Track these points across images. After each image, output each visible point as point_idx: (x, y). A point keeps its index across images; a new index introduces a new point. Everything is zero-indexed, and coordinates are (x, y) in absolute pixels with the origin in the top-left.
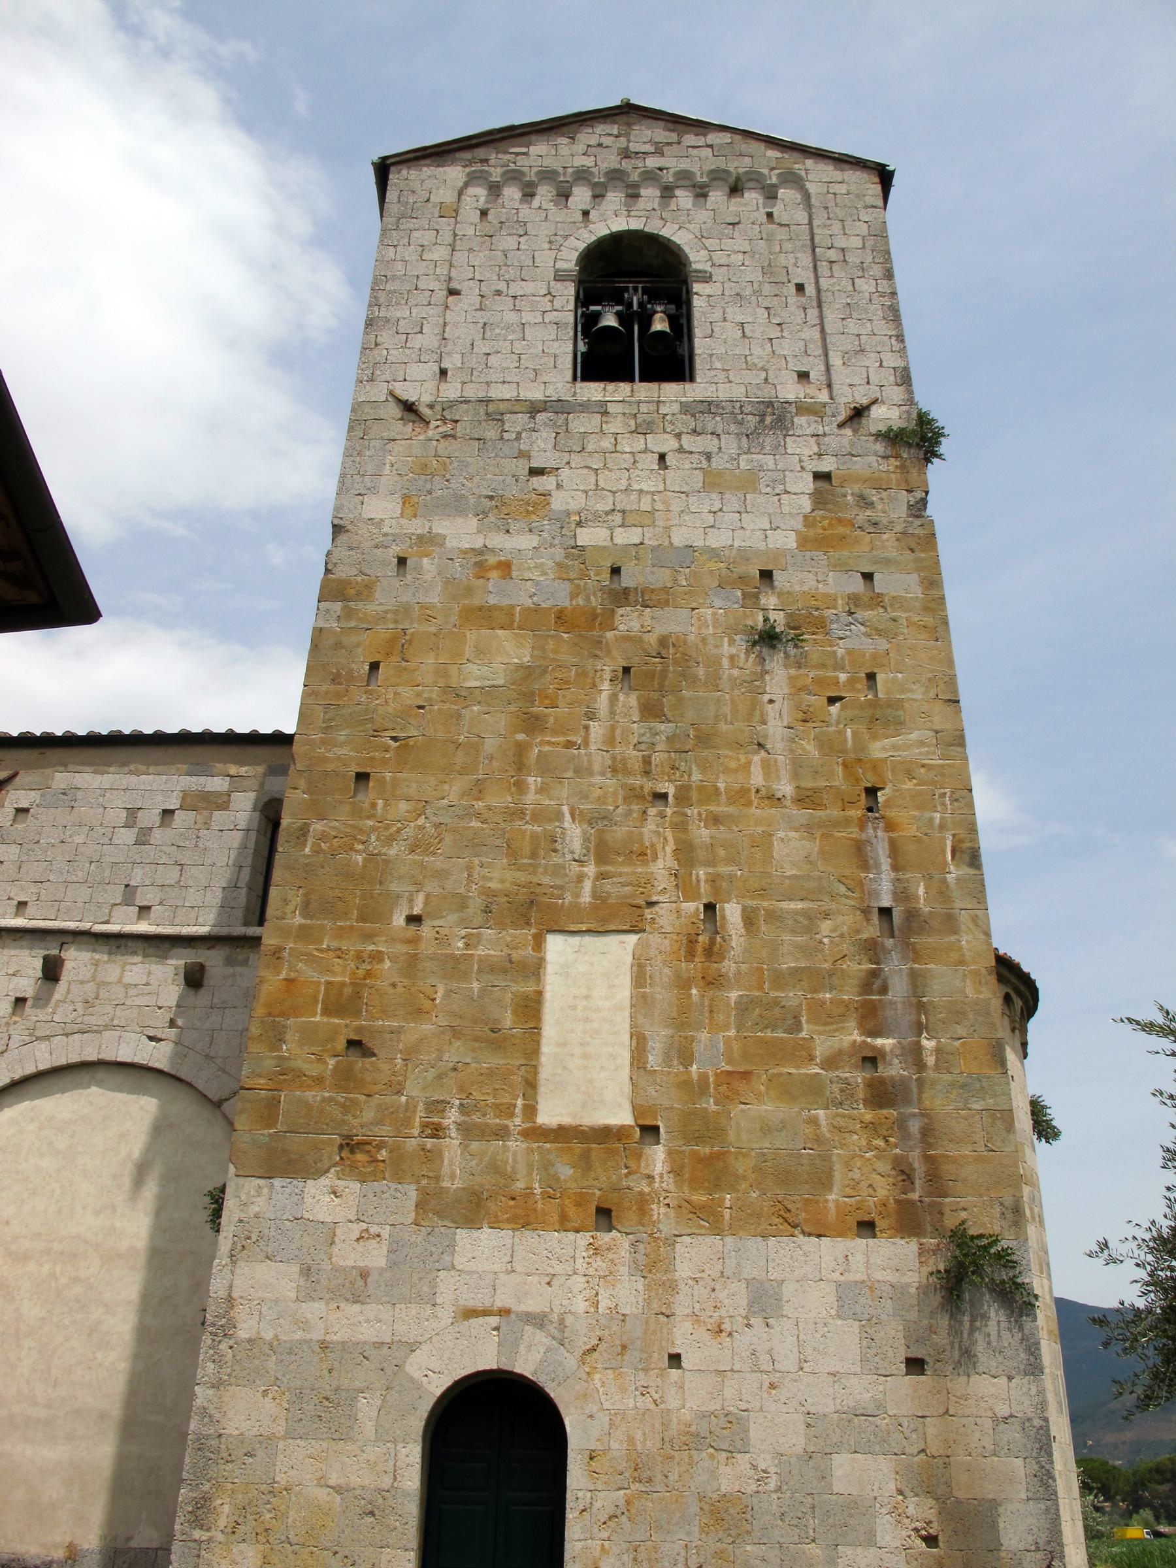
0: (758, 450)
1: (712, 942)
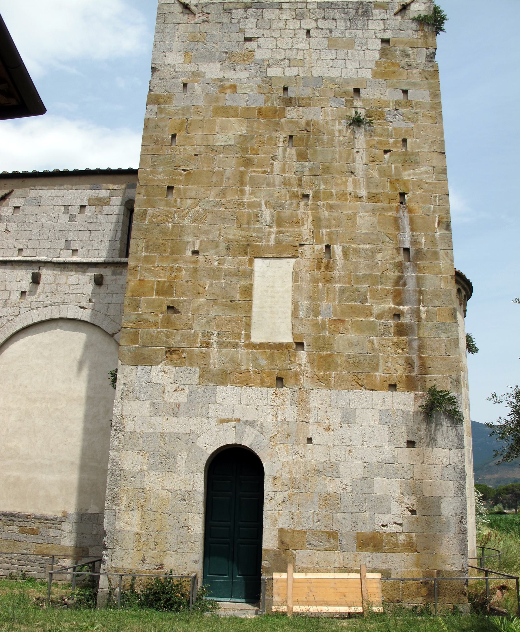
0: (354, 28)
1: (328, 263)
